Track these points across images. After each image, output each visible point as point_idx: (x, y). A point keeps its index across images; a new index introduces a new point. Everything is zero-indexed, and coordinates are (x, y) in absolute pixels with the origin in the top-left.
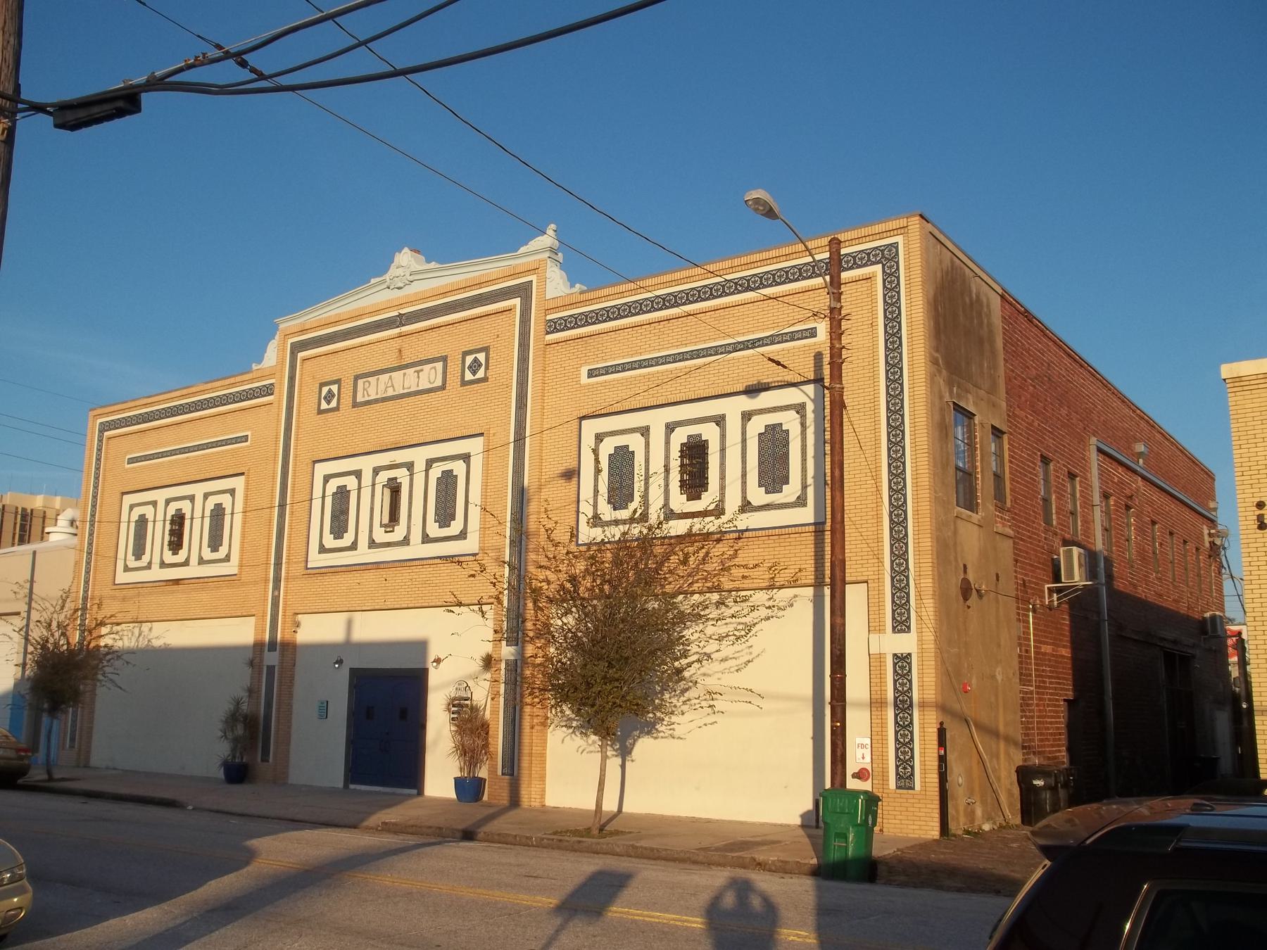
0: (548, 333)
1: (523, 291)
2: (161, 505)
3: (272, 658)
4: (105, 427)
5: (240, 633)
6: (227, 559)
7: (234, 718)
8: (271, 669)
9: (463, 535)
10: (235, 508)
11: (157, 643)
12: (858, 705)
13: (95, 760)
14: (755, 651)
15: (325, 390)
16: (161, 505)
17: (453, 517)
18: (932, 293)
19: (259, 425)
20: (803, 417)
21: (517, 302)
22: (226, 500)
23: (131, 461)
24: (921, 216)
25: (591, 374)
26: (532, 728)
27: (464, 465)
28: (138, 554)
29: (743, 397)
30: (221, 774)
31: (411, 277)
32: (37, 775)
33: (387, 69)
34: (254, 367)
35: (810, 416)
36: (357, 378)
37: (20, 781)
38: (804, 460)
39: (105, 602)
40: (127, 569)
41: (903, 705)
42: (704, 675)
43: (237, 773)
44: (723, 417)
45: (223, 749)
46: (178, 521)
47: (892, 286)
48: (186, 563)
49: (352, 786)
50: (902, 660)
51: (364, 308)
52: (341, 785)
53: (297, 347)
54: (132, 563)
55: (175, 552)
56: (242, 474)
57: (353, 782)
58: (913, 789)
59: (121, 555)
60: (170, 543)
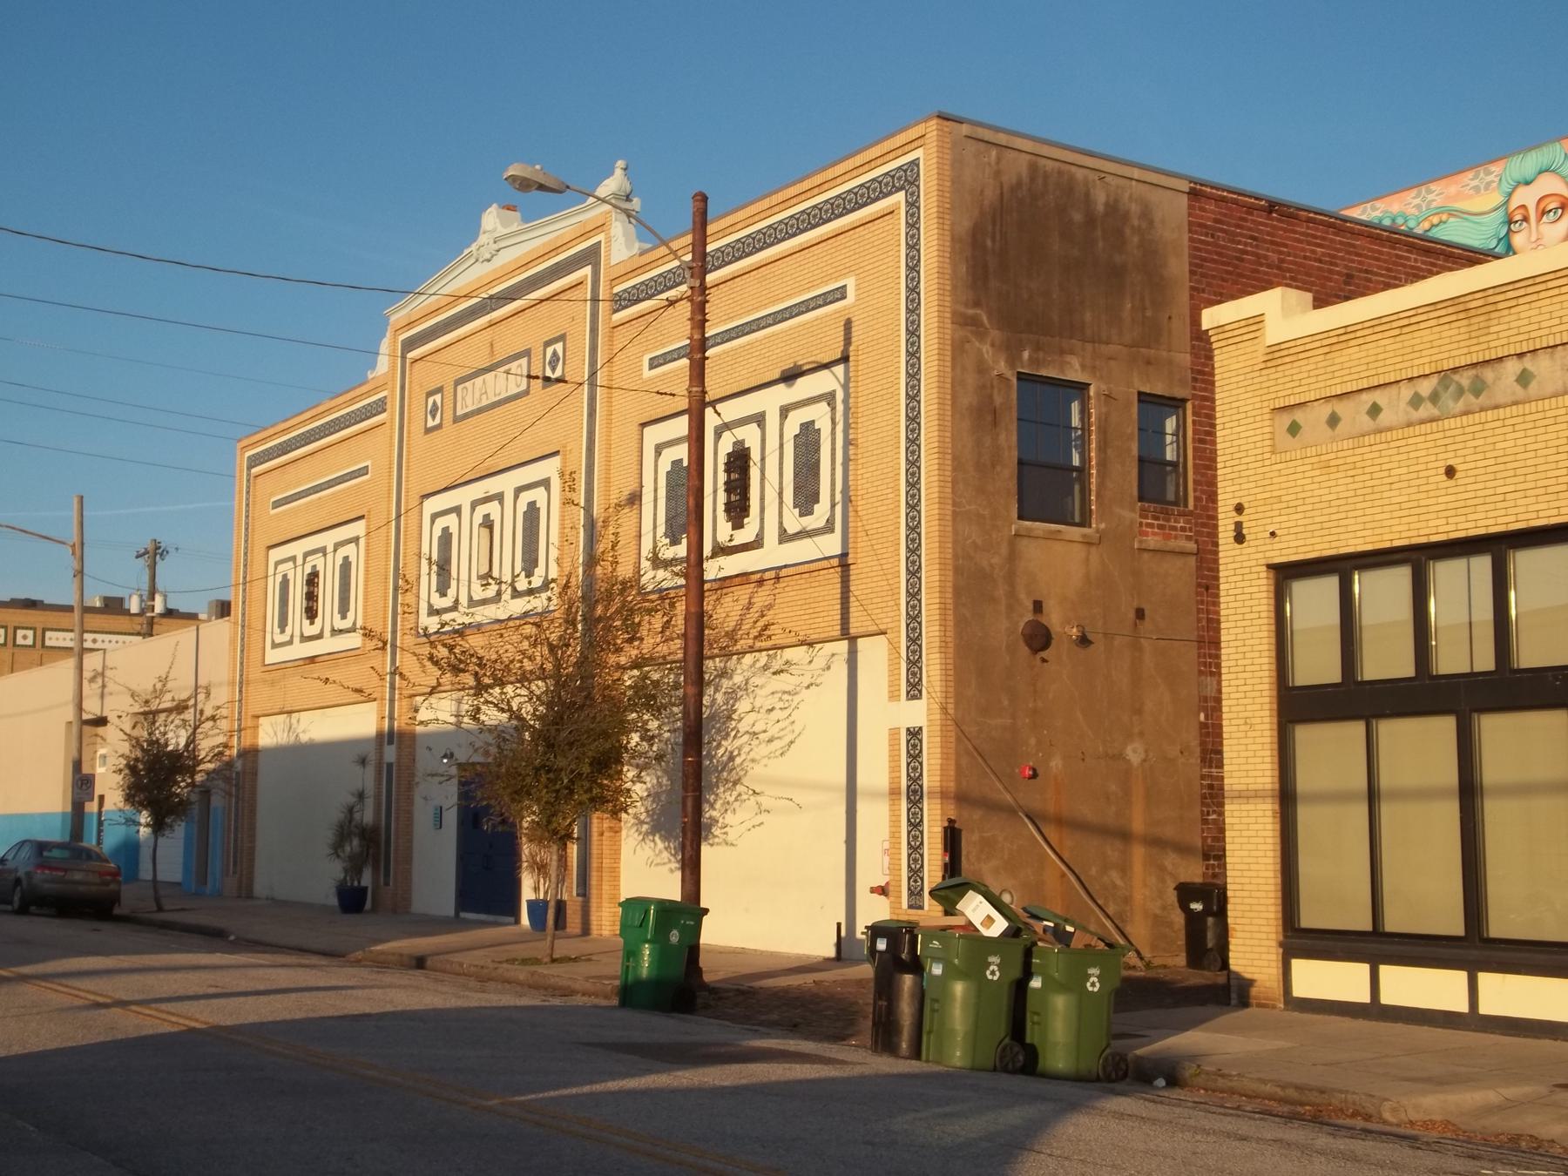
0: (616, 311)
1: (591, 256)
3: (390, 754)
4: (255, 461)
5: (359, 722)
7: (346, 830)
8: (390, 766)
10: (550, 504)
11: (304, 738)
12: (874, 795)
13: (260, 887)
14: (797, 729)
15: (550, 351)
17: (815, 498)
18: (966, 224)
19: (370, 450)
20: (833, 409)
21: (587, 270)
23: (277, 504)
24: (943, 117)
25: (841, 293)
26: (602, 834)
27: (758, 431)
29: (782, 386)
30: (334, 901)
31: (504, 243)
32: (131, 897)
34: (370, 376)
35: (840, 407)
36: (458, 382)
38: (833, 469)
39: (213, 691)
41: (915, 796)
42: (753, 761)
43: (351, 900)
45: (334, 870)
46: (312, 580)
48: (757, 544)
49: (463, 915)
50: (914, 734)
51: (480, 278)
52: (451, 913)
53: (410, 344)
55: (738, 525)
56: (362, 517)
57: (465, 910)
58: (921, 908)
59: (269, 628)
60: (729, 507)
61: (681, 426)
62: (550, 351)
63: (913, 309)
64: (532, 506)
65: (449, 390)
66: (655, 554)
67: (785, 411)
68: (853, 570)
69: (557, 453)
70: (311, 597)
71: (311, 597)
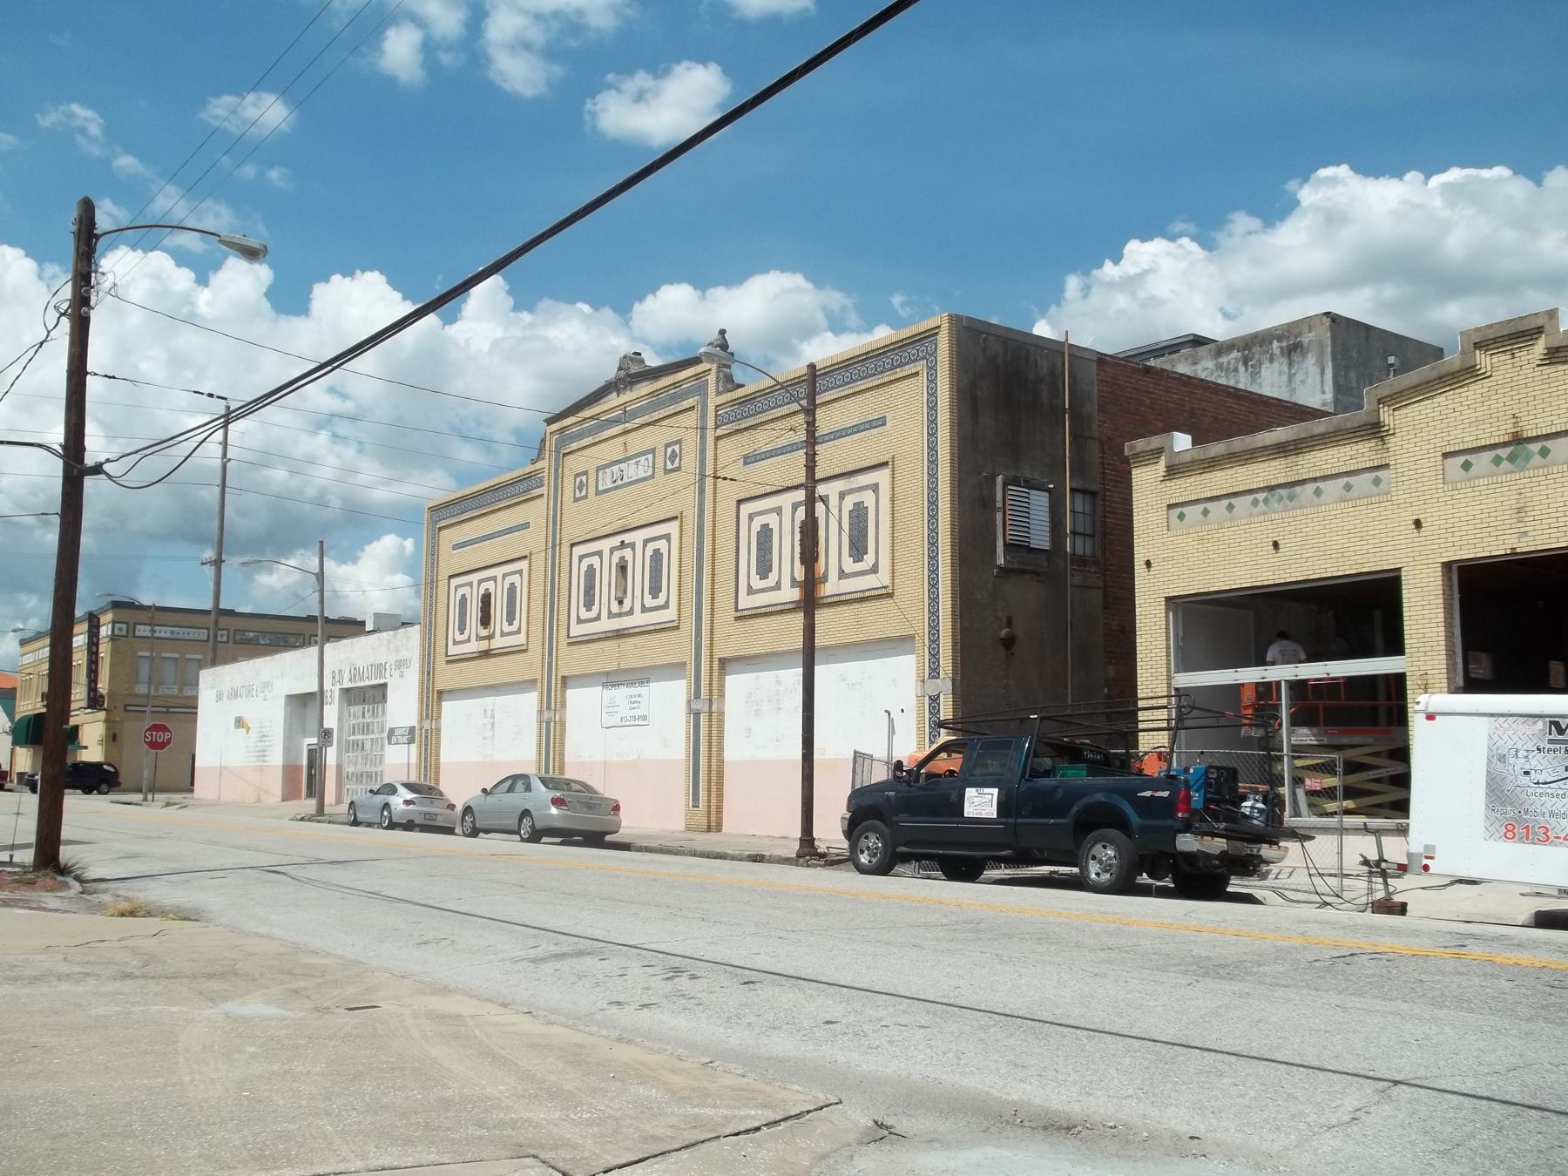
2: (499, 579)
6: (666, 606)
9: (874, 570)
15: (669, 450)
16: (499, 579)
22: (662, 545)
28: (589, 605)
33: (313, 366)
37: (608, 838)
40: (750, 591)
44: (877, 485)
46: (486, 600)
47: (932, 381)
54: (584, 615)
56: (885, 464)
60: (852, 544)
61: (800, 495)
62: (669, 450)
63: (932, 434)
64: (657, 552)
65: (592, 475)
66: (749, 586)
67: (504, 576)
68: (483, 662)
69: (885, 464)
70: (463, 614)
71: (463, 614)
